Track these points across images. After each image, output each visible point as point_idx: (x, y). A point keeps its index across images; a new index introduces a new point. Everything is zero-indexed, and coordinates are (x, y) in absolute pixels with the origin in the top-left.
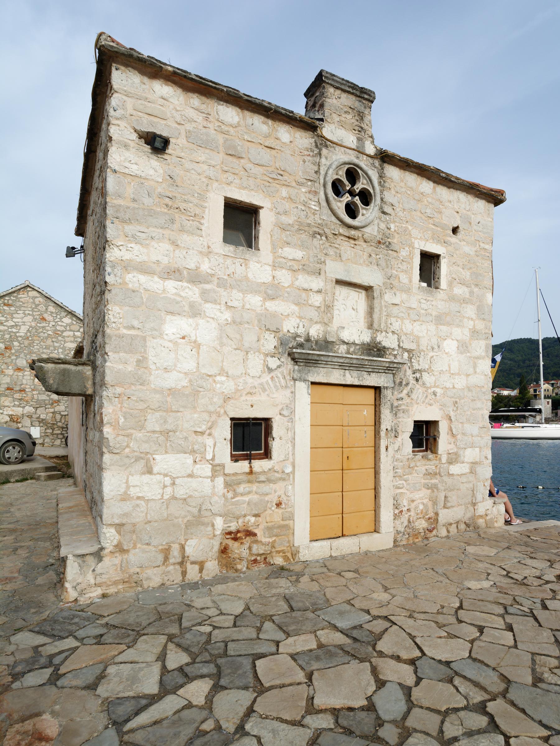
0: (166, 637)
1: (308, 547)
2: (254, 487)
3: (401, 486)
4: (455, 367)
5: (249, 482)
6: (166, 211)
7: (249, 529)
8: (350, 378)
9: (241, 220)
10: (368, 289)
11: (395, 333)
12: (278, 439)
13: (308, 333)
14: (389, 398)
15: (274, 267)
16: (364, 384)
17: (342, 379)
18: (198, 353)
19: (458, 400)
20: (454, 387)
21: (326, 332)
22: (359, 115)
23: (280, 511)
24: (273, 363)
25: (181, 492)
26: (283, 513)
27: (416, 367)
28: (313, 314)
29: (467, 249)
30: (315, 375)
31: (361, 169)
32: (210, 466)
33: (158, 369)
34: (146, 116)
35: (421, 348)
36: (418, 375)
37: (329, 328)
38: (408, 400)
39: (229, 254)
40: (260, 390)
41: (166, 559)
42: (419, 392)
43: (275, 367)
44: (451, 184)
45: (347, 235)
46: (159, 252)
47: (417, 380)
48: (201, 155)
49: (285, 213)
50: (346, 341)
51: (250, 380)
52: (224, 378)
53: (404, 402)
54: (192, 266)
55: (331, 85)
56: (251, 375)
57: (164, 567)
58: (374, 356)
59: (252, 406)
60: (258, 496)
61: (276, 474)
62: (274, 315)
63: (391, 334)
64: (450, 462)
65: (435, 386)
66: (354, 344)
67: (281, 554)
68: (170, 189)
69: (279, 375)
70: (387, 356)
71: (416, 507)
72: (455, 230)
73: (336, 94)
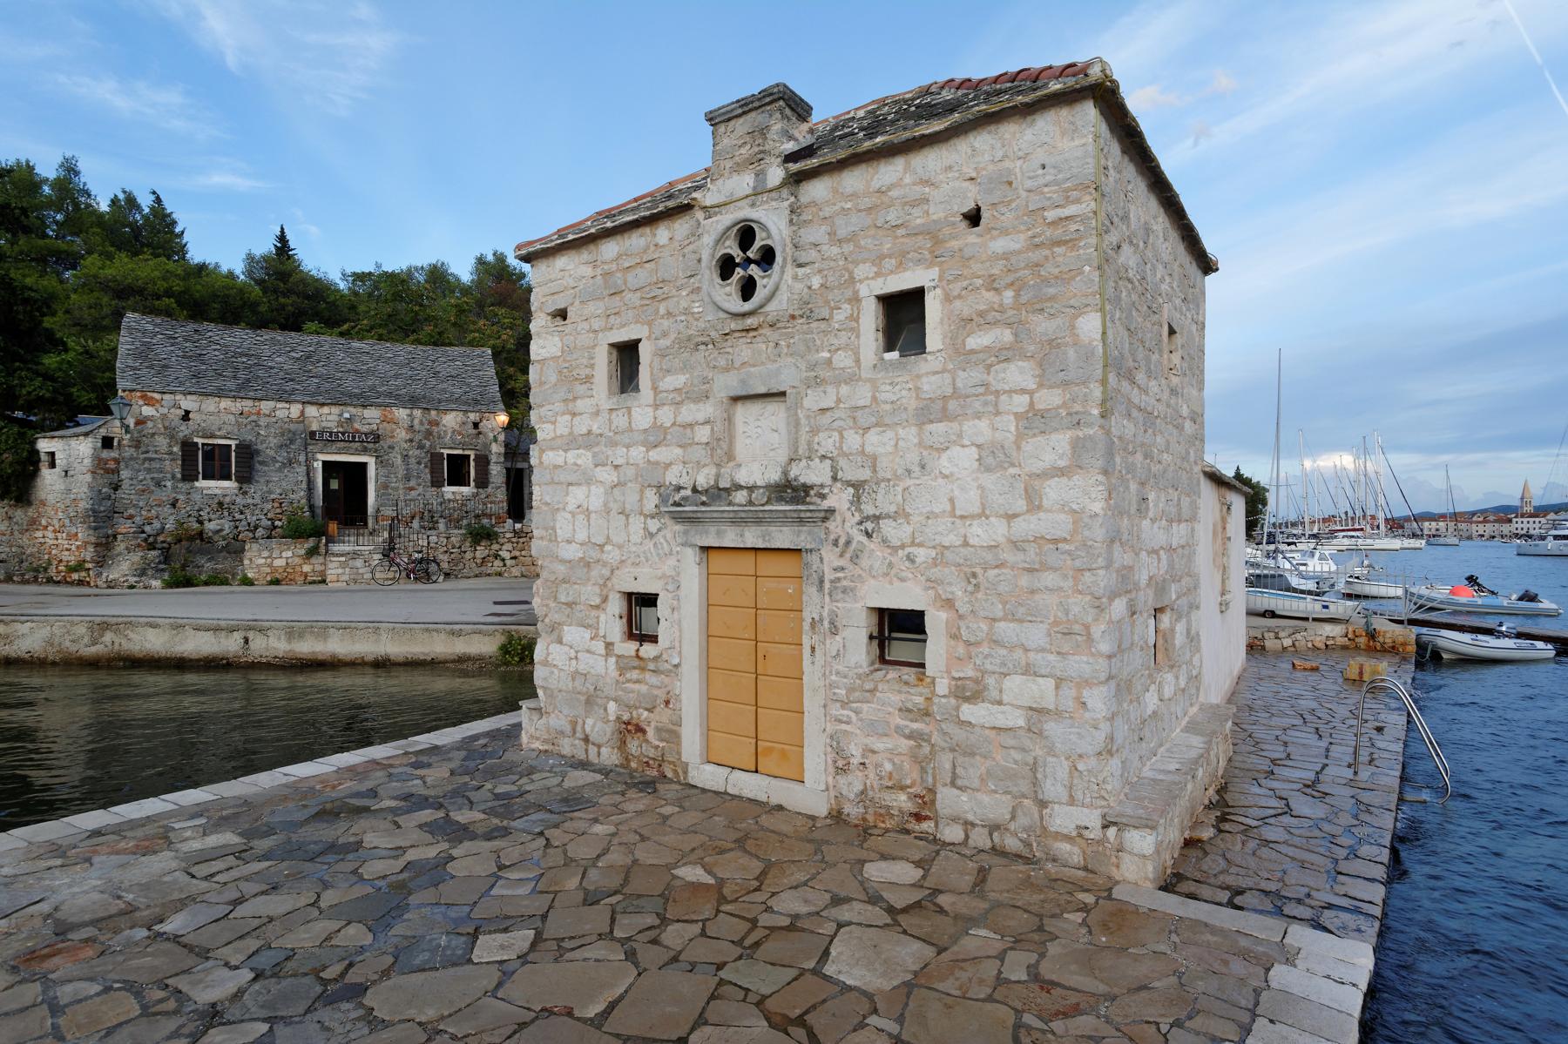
0: (828, 896)
4: (969, 501)
15: (656, 406)
19: (978, 570)
20: (966, 544)
24: (653, 525)
25: (582, 667)
27: (869, 509)
28: (699, 453)
35: (881, 474)
36: (869, 526)
42: (875, 554)
47: (869, 535)
53: (847, 573)
65: (913, 544)
72: (974, 218)
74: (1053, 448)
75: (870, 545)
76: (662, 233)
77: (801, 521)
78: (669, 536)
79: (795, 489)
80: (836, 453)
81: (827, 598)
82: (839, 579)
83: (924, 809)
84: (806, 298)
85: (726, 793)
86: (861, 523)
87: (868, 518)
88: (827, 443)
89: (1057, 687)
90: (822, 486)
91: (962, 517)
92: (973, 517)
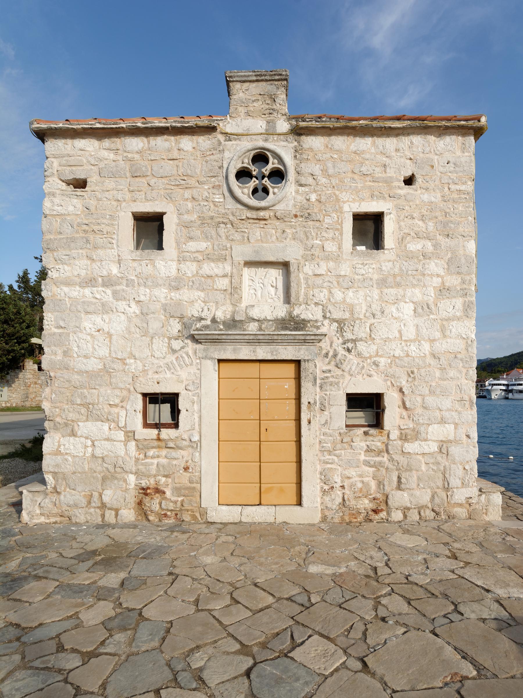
1: (216, 510)
2: (164, 452)
3: (330, 461)
5: (159, 447)
6: (83, 235)
7: (159, 488)
8: (262, 352)
9: (150, 228)
10: (285, 265)
11: (319, 304)
12: (185, 410)
13: (215, 315)
14: (311, 371)
16: (279, 359)
17: (253, 355)
18: (110, 342)
20: (408, 355)
21: (234, 313)
22: (271, 98)
23: (187, 475)
24: (177, 345)
26: (190, 477)
27: (348, 335)
29: (435, 197)
30: (222, 353)
31: (268, 150)
32: (123, 432)
33: (78, 356)
34: (68, 168)
35: (356, 316)
36: (350, 345)
37: (237, 309)
38: (339, 372)
39: (136, 258)
40: (166, 369)
41: (89, 503)
43: (179, 348)
44: (397, 132)
45: (255, 217)
46: (80, 267)
47: (349, 350)
48: (110, 184)
49: (188, 212)
50: (255, 318)
51: (156, 361)
52: (132, 361)
53: (332, 373)
54: (105, 273)
55: (237, 81)
56: (156, 356)
57: (87, 509)
58: (291, 330)
59: (158, 383)
60: (168, 460)
61: (184, 442)
62: (179, 304)
63: (313, 306)
64: (404, 438)
65: (377, 355)
66: (266, 320)
67: (190, 513)
68: (87, 218)
69: (184, 355)
70: (307, 329)
71: (352, 486)
72: (409, 181)
73: (243, 87)
74: (452, 306)
75: (350, 356)
76: (186, 142)
77: (305, 341)
78: (191, 353)
79: (296, 323)
80: (325, 302)
81: (318, 389)
82: (327, 377)
83: (381, 505)
84: (306, 206)
85: (241, 522)
86: (345, 343)
87: (348, 341)
88: (322, 296)
89: (455, 428)
90: (316, 321)
91: (406, 341)
92: (411, 341)
